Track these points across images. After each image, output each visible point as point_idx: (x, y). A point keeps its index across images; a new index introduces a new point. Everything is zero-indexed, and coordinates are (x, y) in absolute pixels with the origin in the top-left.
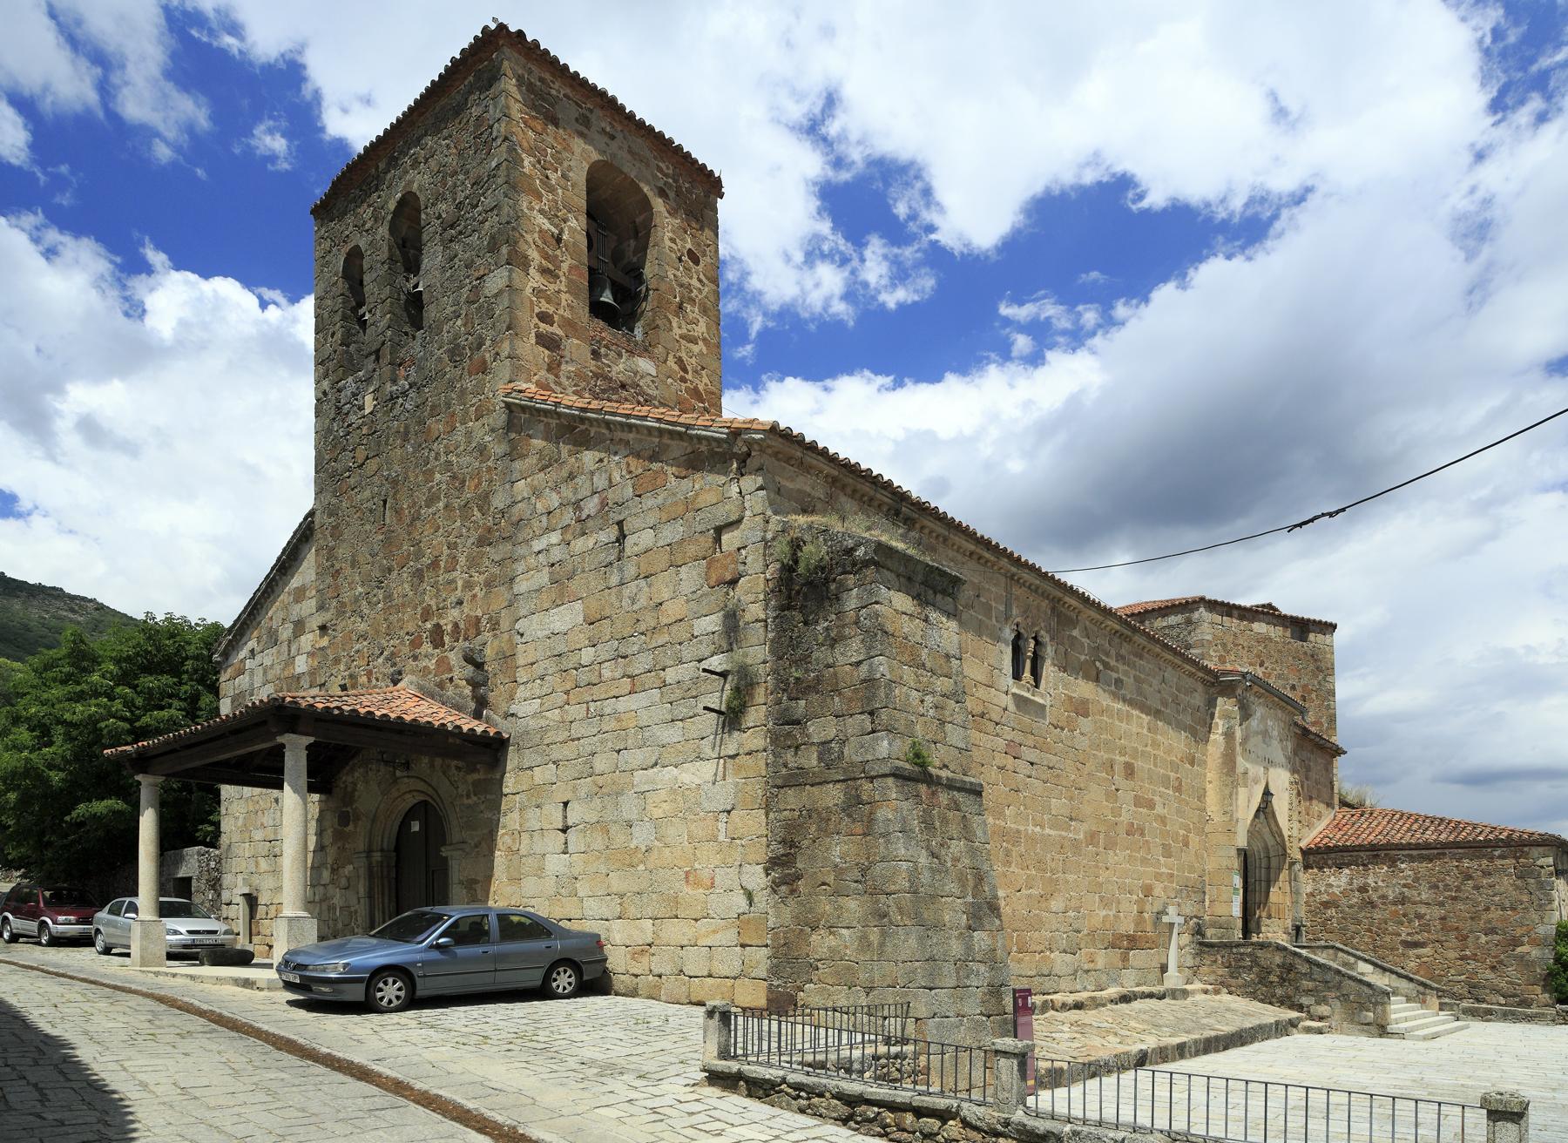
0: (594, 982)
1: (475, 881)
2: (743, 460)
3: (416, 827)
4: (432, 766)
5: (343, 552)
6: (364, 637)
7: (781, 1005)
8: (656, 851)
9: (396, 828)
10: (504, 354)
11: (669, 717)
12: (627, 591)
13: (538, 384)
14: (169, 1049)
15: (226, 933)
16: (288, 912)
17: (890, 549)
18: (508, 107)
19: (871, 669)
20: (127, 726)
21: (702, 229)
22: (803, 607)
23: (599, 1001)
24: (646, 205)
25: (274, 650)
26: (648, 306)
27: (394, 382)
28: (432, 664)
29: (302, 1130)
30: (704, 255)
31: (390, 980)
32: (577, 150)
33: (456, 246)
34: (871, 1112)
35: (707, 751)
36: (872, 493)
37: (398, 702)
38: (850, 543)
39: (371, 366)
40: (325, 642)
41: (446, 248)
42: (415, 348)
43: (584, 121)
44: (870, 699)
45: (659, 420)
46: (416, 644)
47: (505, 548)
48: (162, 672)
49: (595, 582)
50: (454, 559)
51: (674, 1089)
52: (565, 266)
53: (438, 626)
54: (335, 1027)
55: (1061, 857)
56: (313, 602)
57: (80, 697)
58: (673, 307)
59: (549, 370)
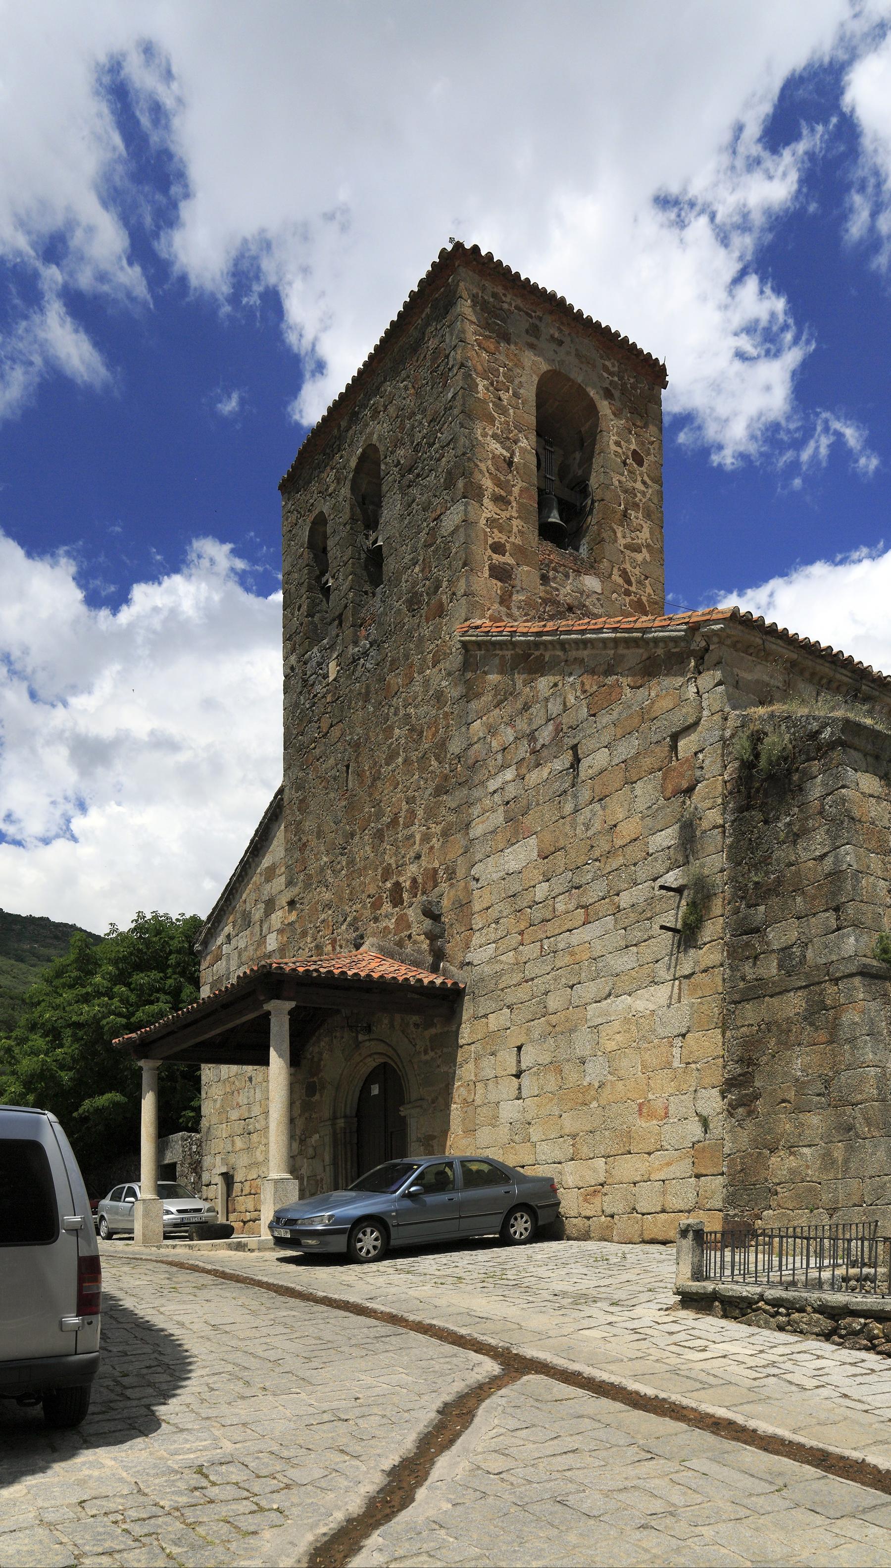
0: (548, 1227)
1: (432, 1137)
2: (701, 657)
3: (375, 1090)
4: (392, 1026)
5: (309, 824)
6: (328, 906)
7: (738, 1235)
8: (609, 1085)
9: (357, 1094)
10: (460, 592)
11: (623, 944)
12: (581, 818)
13: (492, 619)
14: (192, 1298)
15: (209, 1210)
16: (274, 1175)
17: (858, 725)
18: (464, 332)
19: (837, 861)
20: (124, 1021)
21: (646, 426)
22: (764, 804)
23: (554, 1245)
24: (592, 409)
25: (248, 932)
26: (592, 520)
27: (356, 643)
28: (391, 924)
29: (323, 1353)
30: (649, 454)
31: (369, 1230)
32: (527, 363)
33: (414, 491)
34: (857, 1324)
35: (663, 973)
36: (831, 674)
37: (364, 963)
38: (815, 726)
39: (334, 633)
40: (293, 917)
41: (404, 494)
42: (376, 605)
43: (534, 331)
44: (836, 894)
45: (615, 630)
46: (377, 905)
47: (461, 794)
48: (150, 969)
49: (548, 813)
50: (412, 813)
51: (647, 1314)
52: (516, 490)
53: (397, 884)
54: (325, 1276)
56: (282, 879)
57: (86, 999)
58: (618, 516)
59: (501, 603)
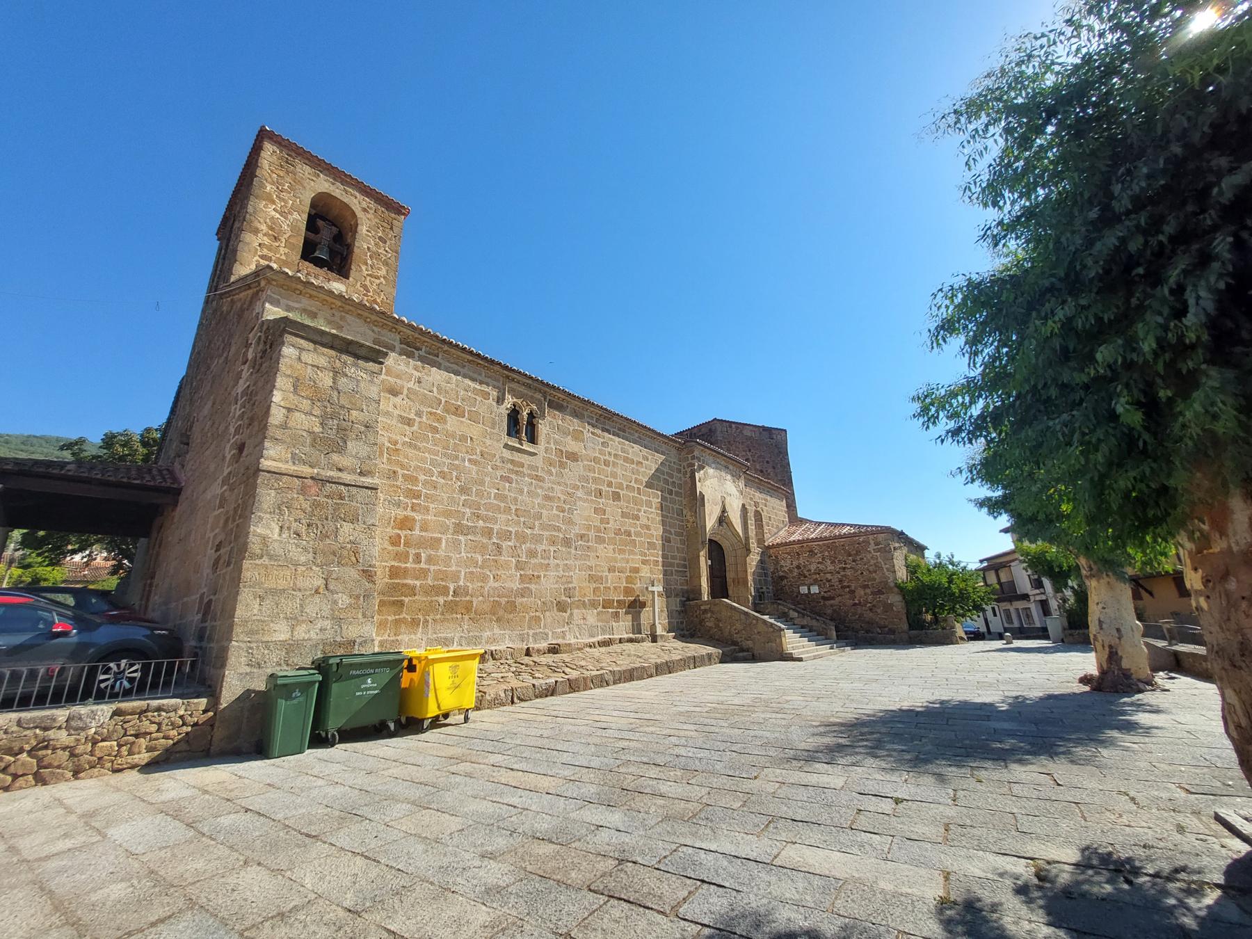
55: (552, 549)
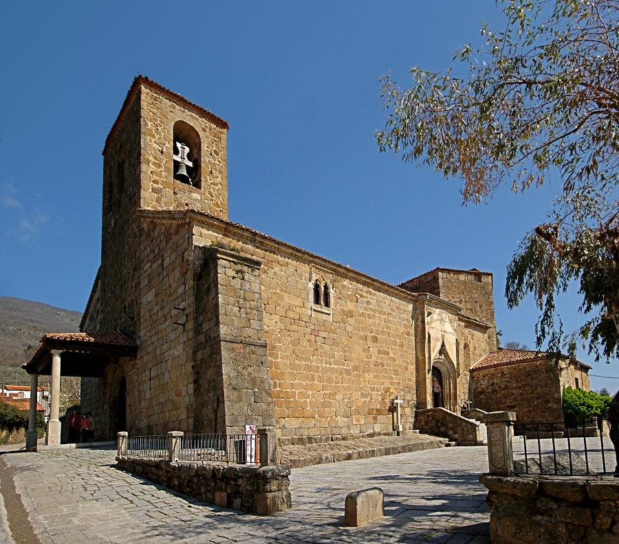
55: (341, 377)
59: (157, 201)
